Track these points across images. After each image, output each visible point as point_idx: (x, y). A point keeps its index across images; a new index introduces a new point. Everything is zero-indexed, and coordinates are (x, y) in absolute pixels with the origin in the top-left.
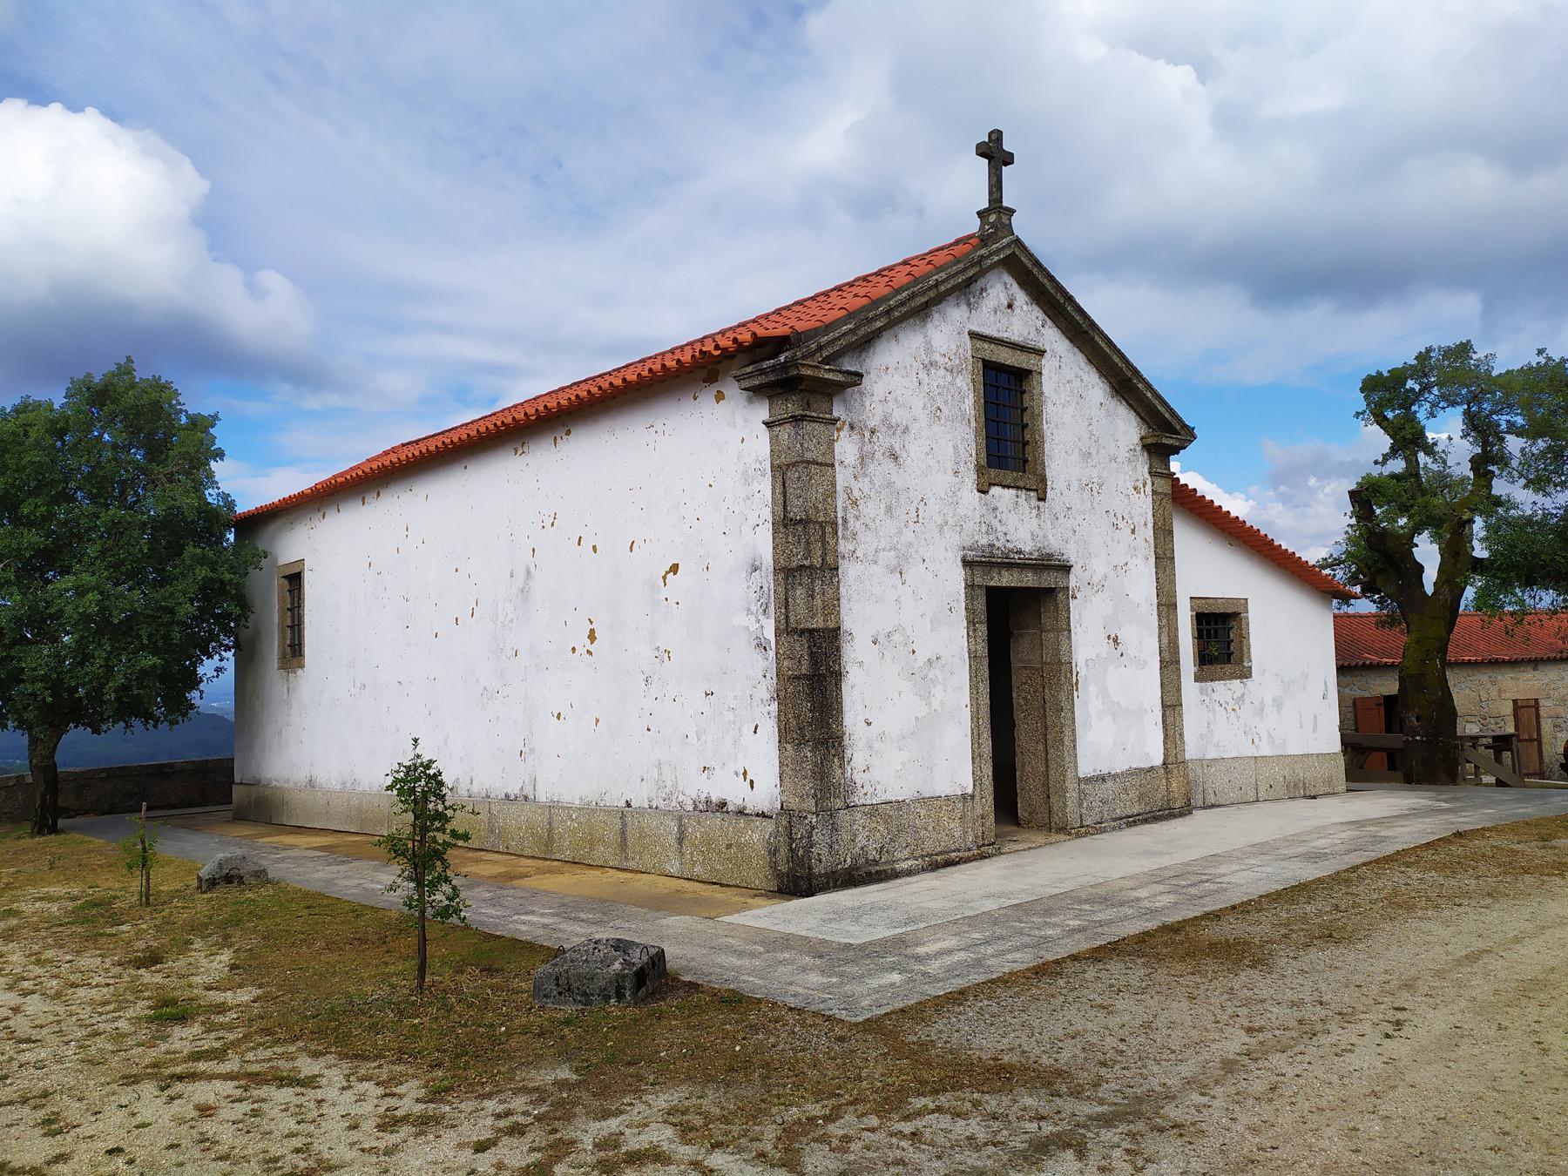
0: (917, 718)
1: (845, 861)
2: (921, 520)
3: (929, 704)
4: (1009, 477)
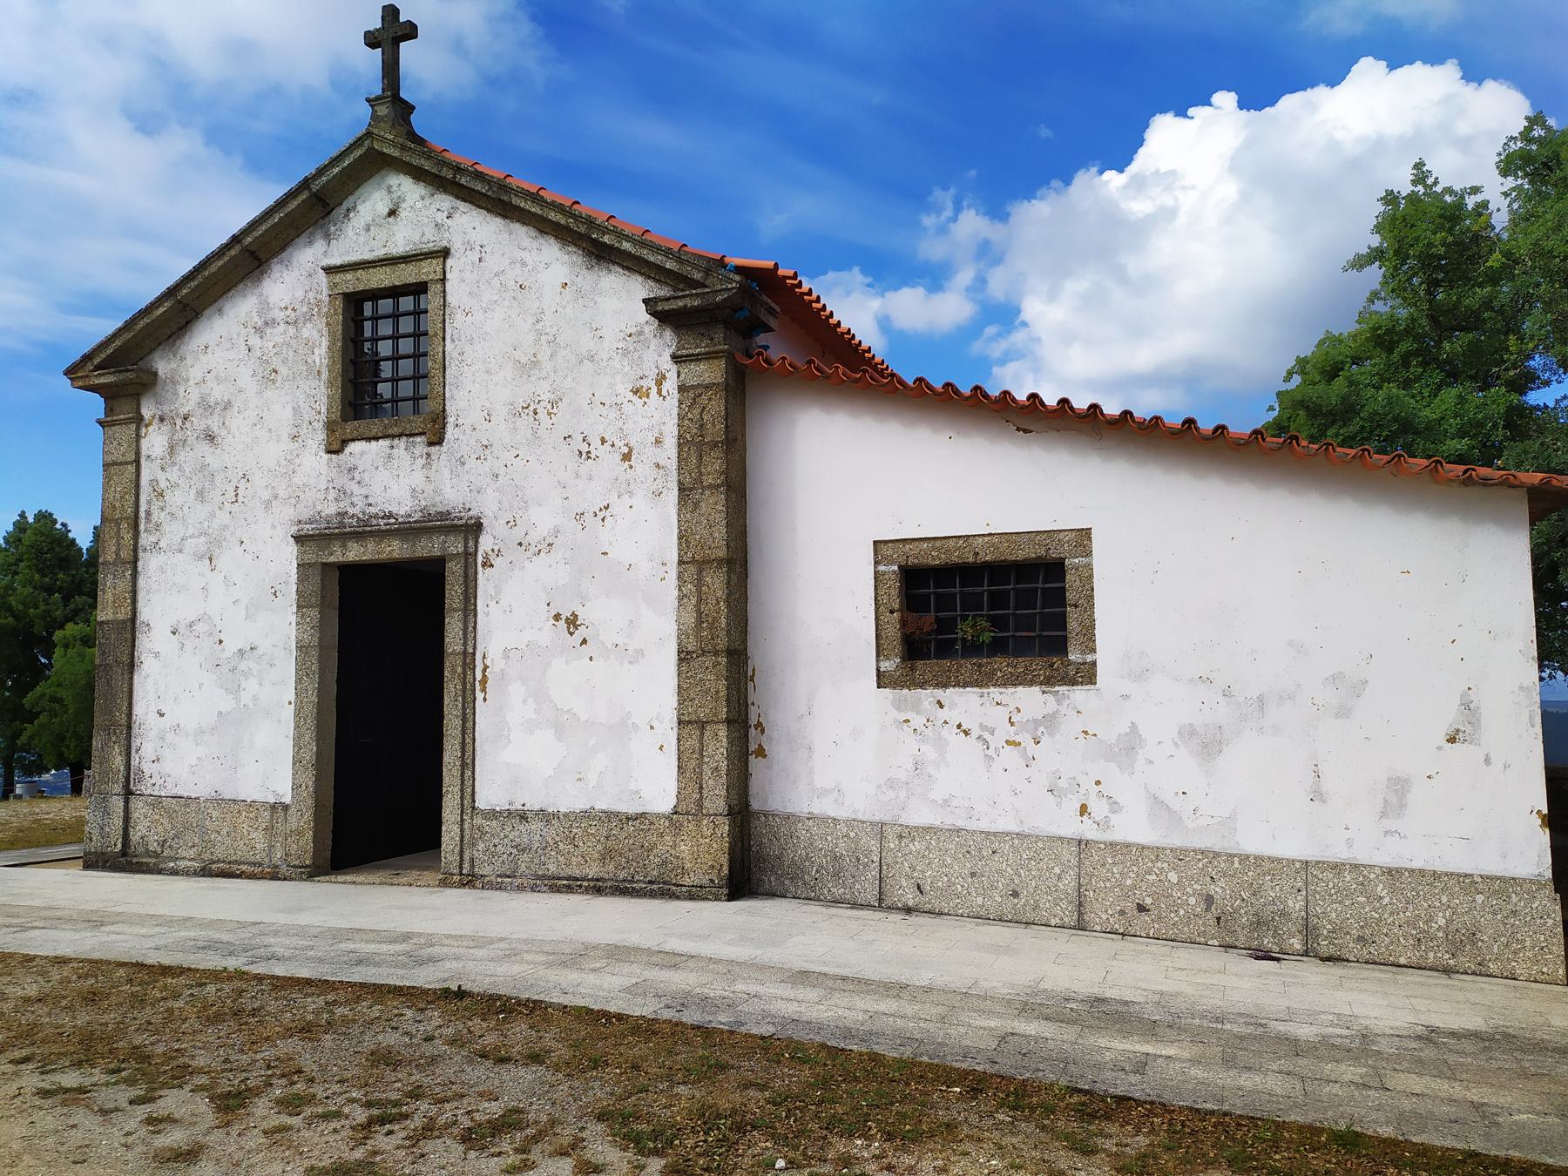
0: (220, 713)
1: (115, 845)
2: (240, 499)
3: (237, 699)
4: (376, 426)
